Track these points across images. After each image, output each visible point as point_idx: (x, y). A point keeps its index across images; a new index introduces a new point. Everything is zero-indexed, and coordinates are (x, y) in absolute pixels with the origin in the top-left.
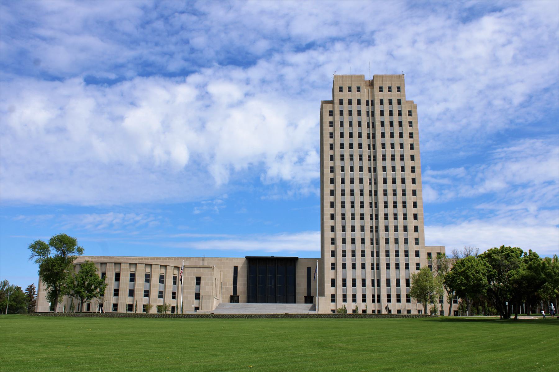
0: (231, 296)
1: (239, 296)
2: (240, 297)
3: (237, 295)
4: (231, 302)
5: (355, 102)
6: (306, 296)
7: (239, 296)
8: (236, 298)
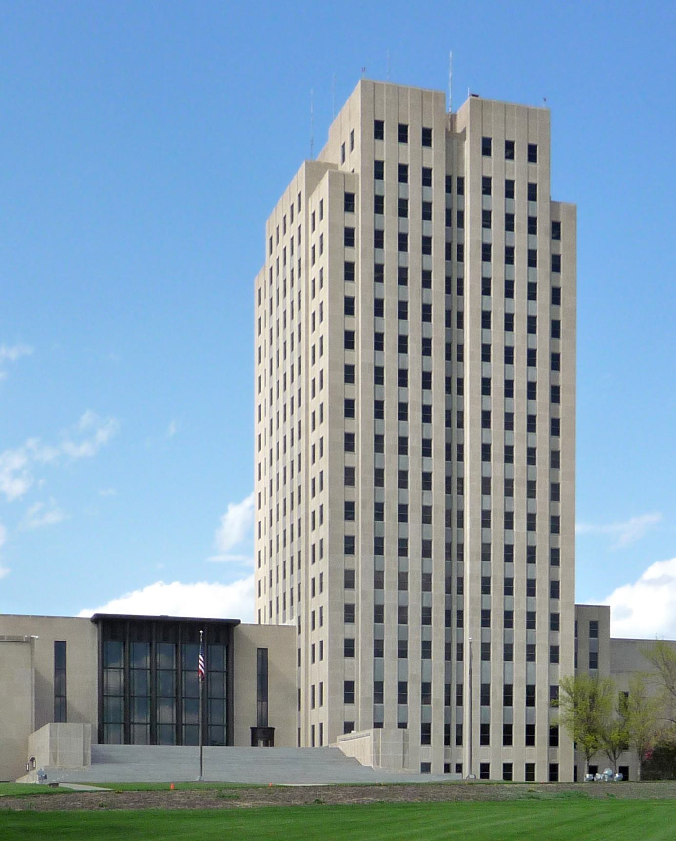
5: (414, 176)
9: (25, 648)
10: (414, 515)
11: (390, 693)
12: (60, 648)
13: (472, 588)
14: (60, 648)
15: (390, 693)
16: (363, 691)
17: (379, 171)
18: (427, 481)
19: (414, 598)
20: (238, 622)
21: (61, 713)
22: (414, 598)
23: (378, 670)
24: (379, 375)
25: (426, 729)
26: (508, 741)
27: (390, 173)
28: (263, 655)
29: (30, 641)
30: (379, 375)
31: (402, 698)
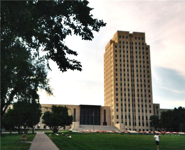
5: (125, 43)
9: (70, 110)
10: (127, 90)
11: (124, 117)
12: (75, 110)
13: (136, 101)
14: (75, 110)
15: (124, 117)
16: (120, 117)
17: (120, 42)
18: (128, 85)
19: (127, 92)
20: (101, 106)
21: (122, 123)
22: (127, 92)
23: (122, 114)
24: (121, 61)
25: (126, 123)
26: (140, 125)
27: (122, 42)
28: (105, 111)
29: (71, 109)
30: (121, 61)
31: (126, 118)
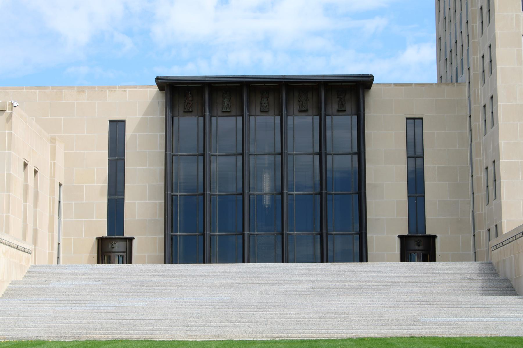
0: (101, 241)
1: (131, 239)
2: (134, 242)
3: (126, 235)
4: (100, 261)
6: (105, 234)
7: (131, 239)
8: (119, 247)
